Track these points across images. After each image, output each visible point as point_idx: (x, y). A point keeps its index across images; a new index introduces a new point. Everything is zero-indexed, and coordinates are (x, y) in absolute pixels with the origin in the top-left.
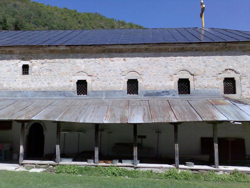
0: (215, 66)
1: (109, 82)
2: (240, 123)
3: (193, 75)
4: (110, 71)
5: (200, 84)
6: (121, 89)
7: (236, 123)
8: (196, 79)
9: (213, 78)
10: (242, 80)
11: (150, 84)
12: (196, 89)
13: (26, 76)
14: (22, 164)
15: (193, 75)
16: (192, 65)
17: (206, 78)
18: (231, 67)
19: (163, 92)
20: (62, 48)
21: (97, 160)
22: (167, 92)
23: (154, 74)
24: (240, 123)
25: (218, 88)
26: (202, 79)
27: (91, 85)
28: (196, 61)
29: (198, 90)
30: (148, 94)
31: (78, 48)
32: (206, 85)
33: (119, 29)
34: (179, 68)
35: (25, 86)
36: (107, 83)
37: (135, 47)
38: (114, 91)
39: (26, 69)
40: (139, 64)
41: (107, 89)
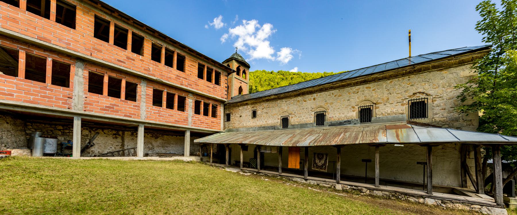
0: (400, 92)
1: (303, 117)
2: (403, 146)
3: (376, 104)
4: (303, 109)
5: (382, 111)
6: (311, 122)
7: (396, 145)
8: (378, 107)
9: (397, 104)
10: (436, 103)
11: (334, 116)
12: (378, 116)
13: (255, 119)
14: (242, 170)
15: (376, 104)
16: (374, 95)
17: (389, 105)
18: (421, 90)
19: (345, 122)
20: (272, 97)
21: (280, 171)
22: (349, 121)
23: (338, 107)
24: (403, 146)
25: (403, 114)
26: (385, 106)
27: (292, 121)
28: (379, 91)
29: (379, 118)
30: (332, 125)
31: (282, 96)
32: (389, 112)
33: (469, 121)
34: (361, 99)
35: (254, 124)
36: (301, 119)
37: (321, 87)
38: (306, 124)
39: (254, 114)
40: (326, 101)
41: (301, 123)
